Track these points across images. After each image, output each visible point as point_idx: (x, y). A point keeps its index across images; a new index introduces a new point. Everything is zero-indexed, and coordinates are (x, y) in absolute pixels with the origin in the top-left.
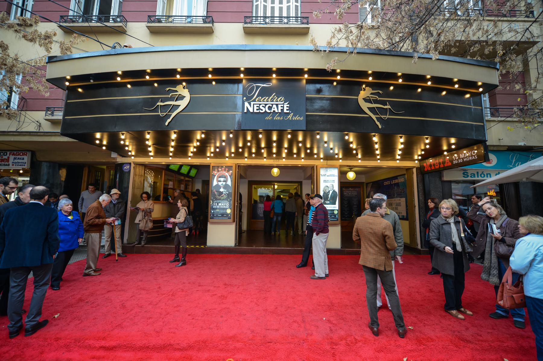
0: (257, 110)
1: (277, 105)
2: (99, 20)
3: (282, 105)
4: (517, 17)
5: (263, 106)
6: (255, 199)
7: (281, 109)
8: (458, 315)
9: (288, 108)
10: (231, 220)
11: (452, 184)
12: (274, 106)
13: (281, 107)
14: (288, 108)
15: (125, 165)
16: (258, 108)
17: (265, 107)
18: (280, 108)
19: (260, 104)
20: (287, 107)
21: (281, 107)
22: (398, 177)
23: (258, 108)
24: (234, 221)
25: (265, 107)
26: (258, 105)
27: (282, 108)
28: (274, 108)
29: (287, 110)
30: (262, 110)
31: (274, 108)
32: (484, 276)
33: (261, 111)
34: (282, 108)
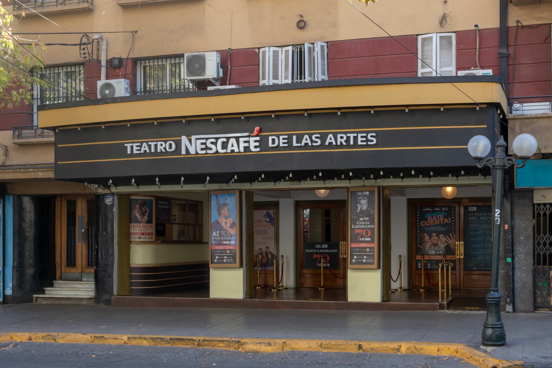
0: (202, 149)
1: (237, 139)
2: (349, 137)
3: (246, 139)
4: (149, 338)
5: (212, 143)
6: (501, 301)
7: (245, 147)
8: (225, 202)
9: (257, 144)
10: (375, 266)
11: (240, 139)
12: (233, 141)
13: (245, 142)
14: (257, 144)
15: (107, 196)
16: (204, 146)
17: (215, 144)
18: (242, 145)
19: (207, 139)
20: (256, 141)
21: (245, 142)
22: (54, 78)
23: (204, 146)
24: (379, 267)
25: (215, 144)
26: (204, 141)
27: (246, 145)
28: (233, 146)
29: (256, 147)
30: (211, 149)
31: (233, 146)
32: (510, 295)
33: (209, 152)
34: (246, 145)
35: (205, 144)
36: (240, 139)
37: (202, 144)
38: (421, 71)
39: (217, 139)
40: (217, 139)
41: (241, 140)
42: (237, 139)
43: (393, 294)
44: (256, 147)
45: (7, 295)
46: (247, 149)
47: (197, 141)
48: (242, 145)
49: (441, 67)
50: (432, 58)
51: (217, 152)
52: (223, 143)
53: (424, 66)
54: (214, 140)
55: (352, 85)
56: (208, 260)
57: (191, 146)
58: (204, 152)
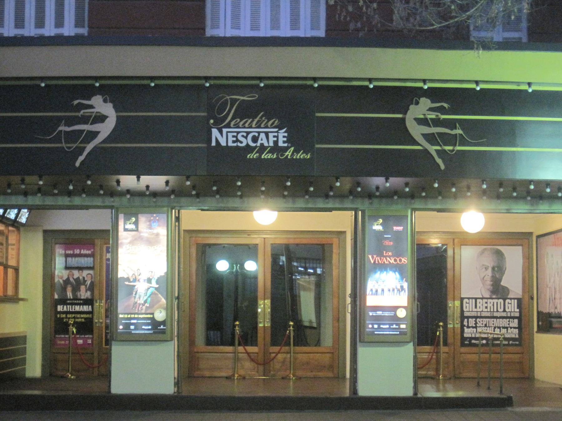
0: (234, 142)
1: (267, 134)
3: (276, 134)
5: (243, 136)
9: (285, 139)
12: (263, 136)
14: (285, 139)
16: (235, 139)
17: (246, 138)
21: (274, 137)
23: (235, 139)
25: (246, 138)
26: (235, 134)
27: (275, 139)
29: (284, 142)
30: (241, 142)
31: (262, 140)
33: (239, 144)
35: (236, 137)
36: (270, 134)
37: (233, 136)
38: (209, 32)
39: (248, 133)
40: (248, 133)
41: (271, 135)
42: (267, 134)
43: (150, 188)
44: (284, 142)
45: (138, 215)
46: (276, 143)
47: (229, 134)
48: (272, 139)
49: (312, 22)
50: (251, 18)
51: (248, 145)
52: (254, 137)
53: (213, 27)
54: (245, 134)
55: (541, 83)
56: (284, 246)
57: (221, 137)
58: (235, 145)
